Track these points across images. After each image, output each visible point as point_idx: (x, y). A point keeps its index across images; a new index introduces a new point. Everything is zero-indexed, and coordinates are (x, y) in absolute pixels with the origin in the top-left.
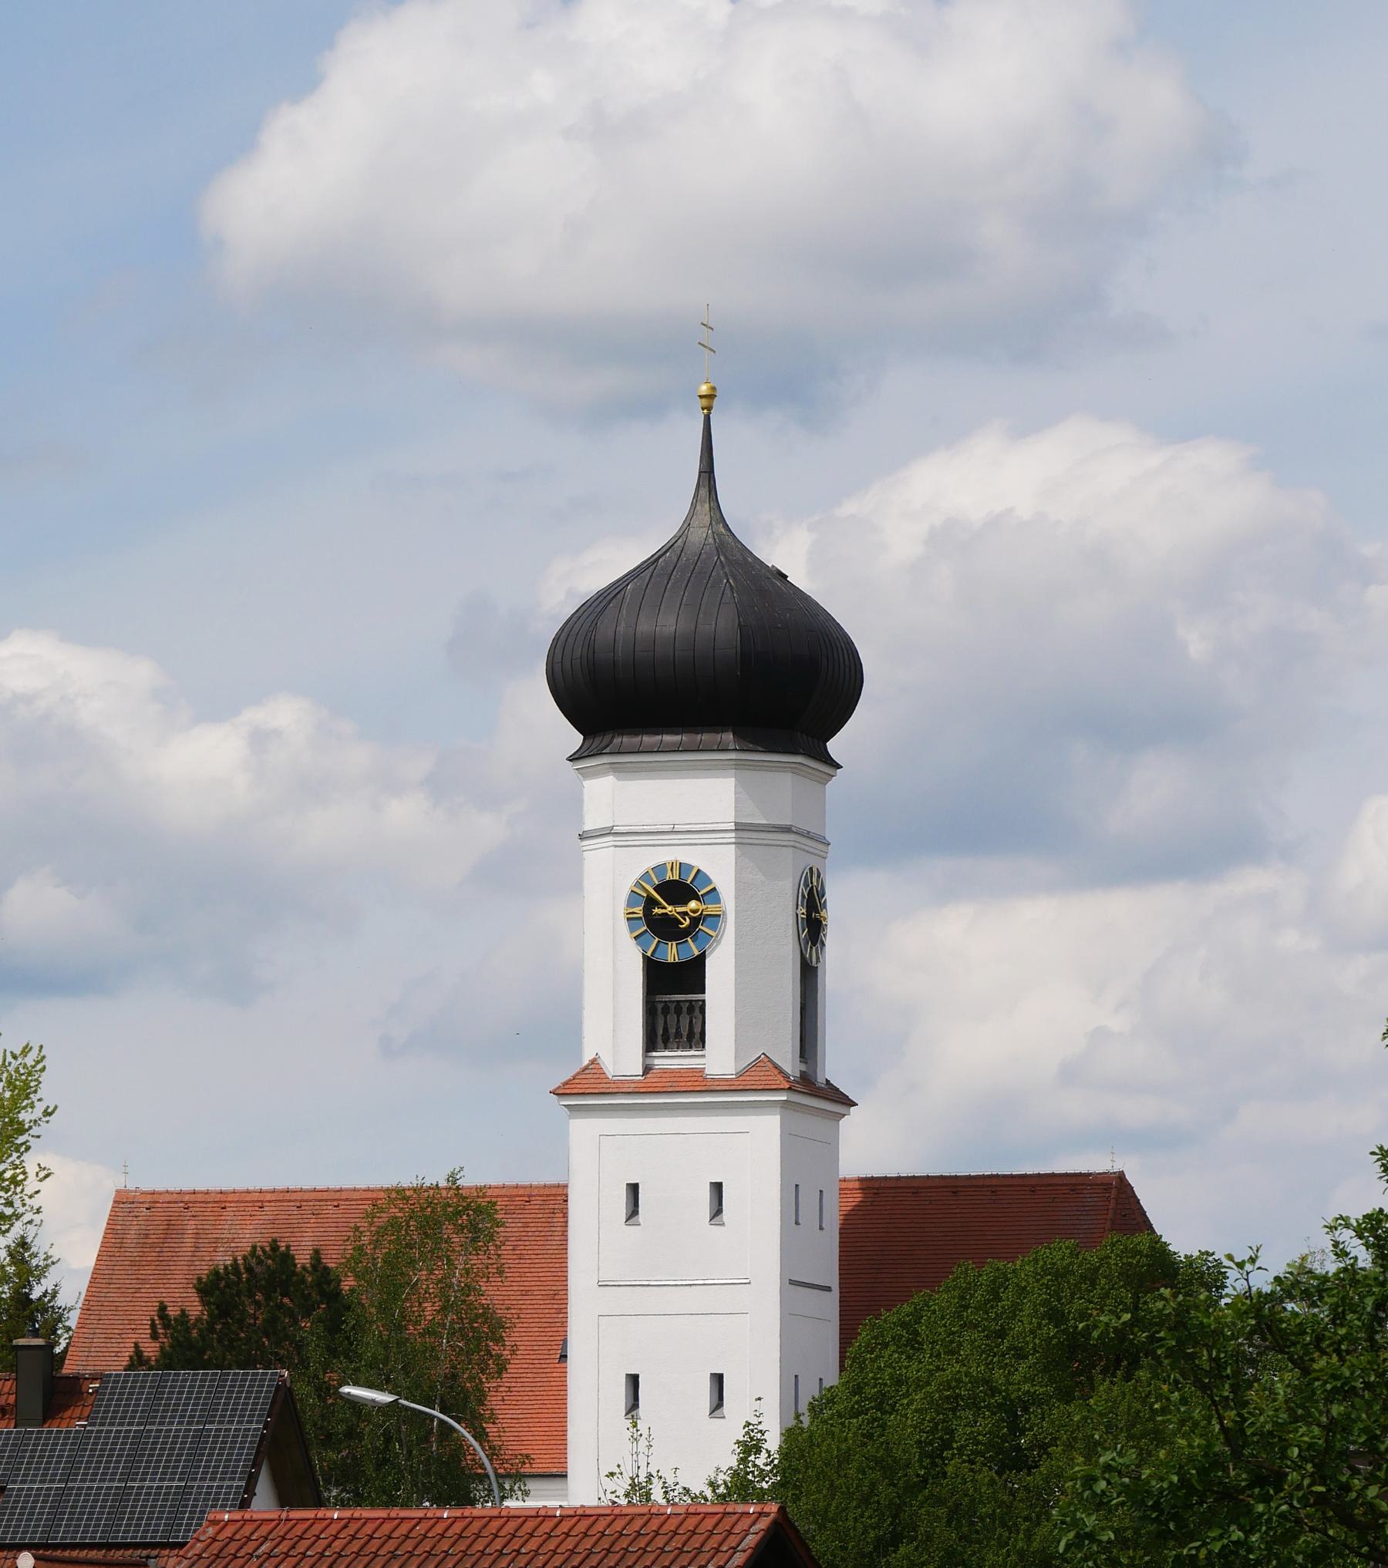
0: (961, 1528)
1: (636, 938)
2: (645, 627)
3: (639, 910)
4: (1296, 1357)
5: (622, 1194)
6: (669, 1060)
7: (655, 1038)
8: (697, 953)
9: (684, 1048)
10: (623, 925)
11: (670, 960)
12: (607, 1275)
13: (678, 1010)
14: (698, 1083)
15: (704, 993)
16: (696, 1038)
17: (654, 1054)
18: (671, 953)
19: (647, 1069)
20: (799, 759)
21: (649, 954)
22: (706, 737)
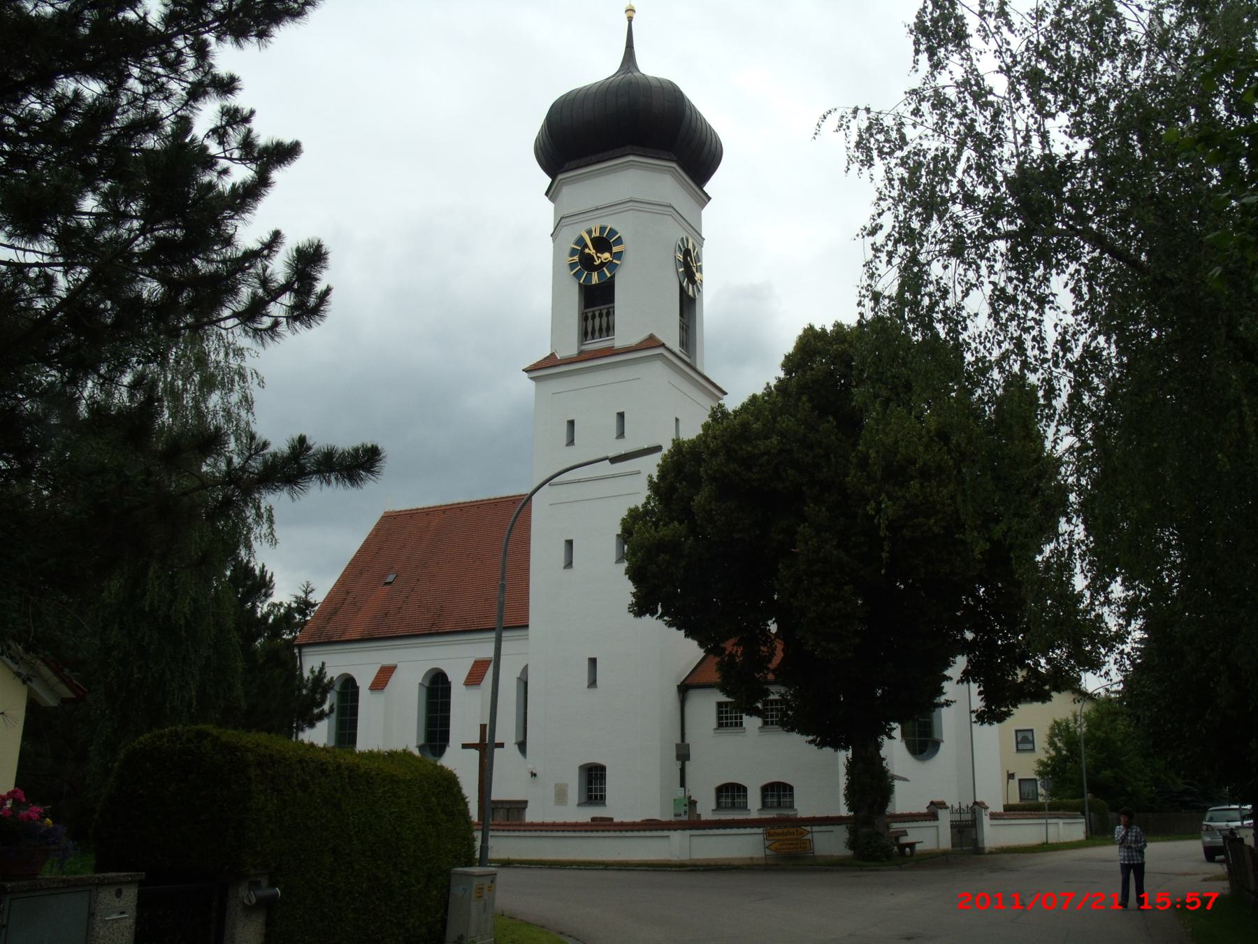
15: (612, 301)
21: (581, 282)
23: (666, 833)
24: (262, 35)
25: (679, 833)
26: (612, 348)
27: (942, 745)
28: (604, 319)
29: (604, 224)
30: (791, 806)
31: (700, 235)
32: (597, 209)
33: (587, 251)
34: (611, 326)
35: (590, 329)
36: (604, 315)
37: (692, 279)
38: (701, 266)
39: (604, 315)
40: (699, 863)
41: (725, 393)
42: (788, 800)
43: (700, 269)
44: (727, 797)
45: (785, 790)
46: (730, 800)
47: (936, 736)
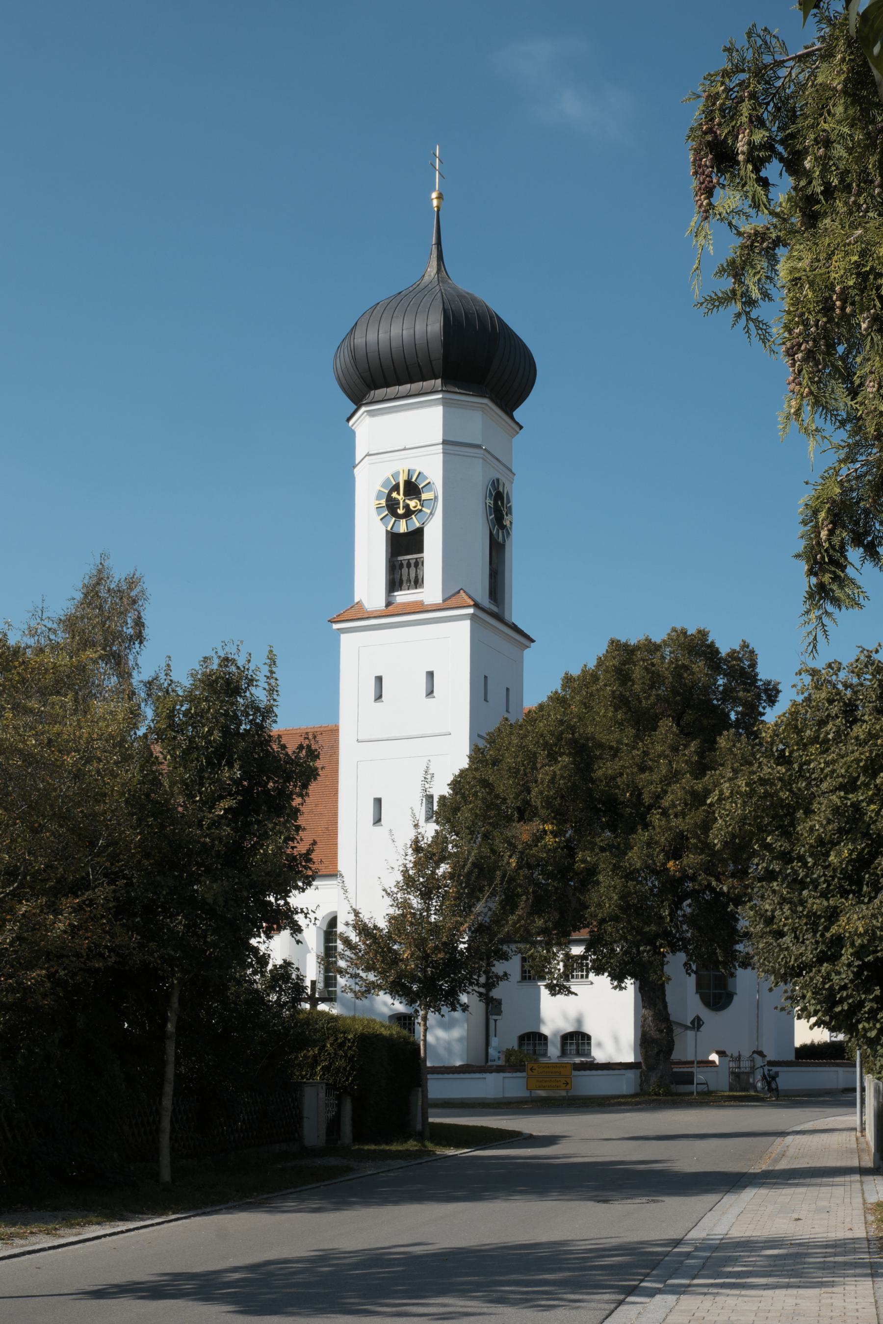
0: (761, 785)
1: (381, 519)
2: (372, 337)
3: (383, 502)
4: (36, 825)
5: (372, 683)
6: (403, 597)
7: (394, 584)
8: (418, 525)
9: (413, 589)
10: (374, 512)
11: (402, 531)
12: (360, 738)
13: (409, 565)
14: (419, 608)
15: (421, 550)
16: (418, 583)
17: (396, 594)
18: (402, 527)
19: (389, 604)
20: (486, 401)
21: (389, 529)
22: (824, 1180)
23: (485, 1075)
24: (568, 680)
25: (494, 1075)
26: (421, 603)
27: (735, 998)
28: (413, 570)
29: (412, 467)
30: (589, 1054)
31: (511, 471)
32: (405, 449)
33: (394, 495)
34: (420, 580)
35: (397, 580)
36: (413, 565)
37: (502, 527)
38: (510, 507)
39: (413, 565)
40: (639, 1081)
41: (533, 641)
42: (542, 1048)
43: (509, 511)
44: (571, 1044)
45: (540, 1039)
46: (531, 1048)
47: (730, 989)
